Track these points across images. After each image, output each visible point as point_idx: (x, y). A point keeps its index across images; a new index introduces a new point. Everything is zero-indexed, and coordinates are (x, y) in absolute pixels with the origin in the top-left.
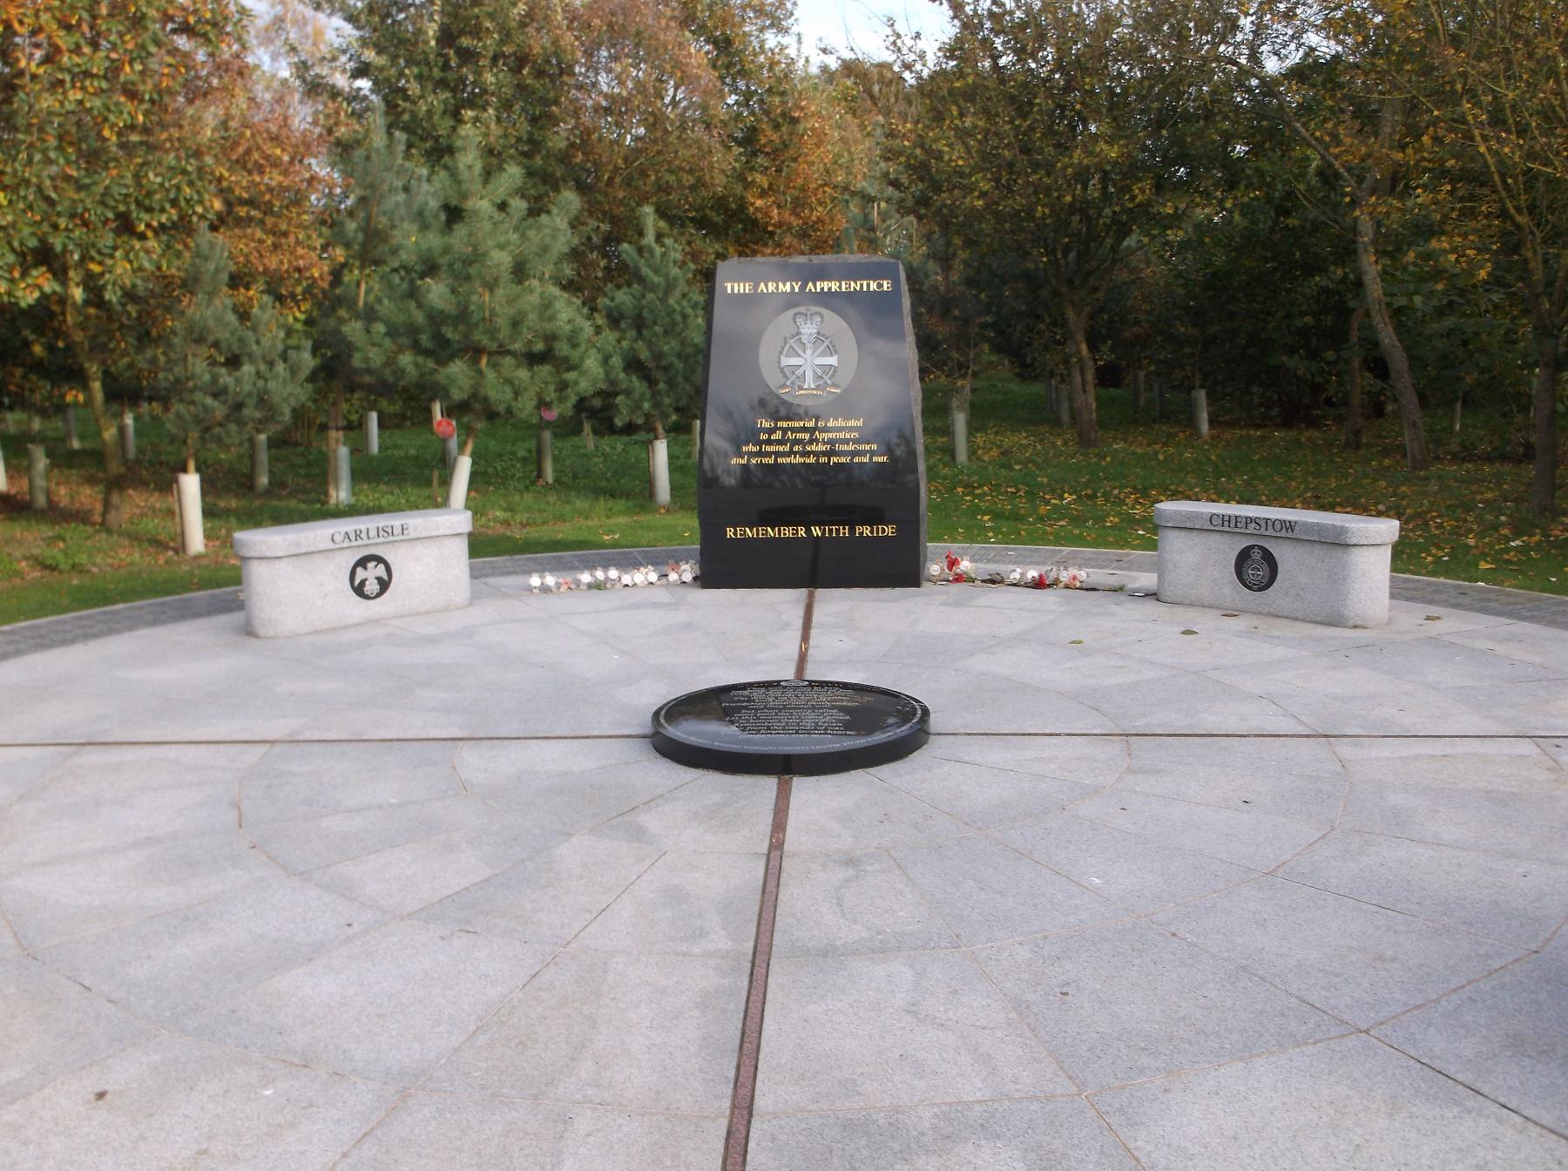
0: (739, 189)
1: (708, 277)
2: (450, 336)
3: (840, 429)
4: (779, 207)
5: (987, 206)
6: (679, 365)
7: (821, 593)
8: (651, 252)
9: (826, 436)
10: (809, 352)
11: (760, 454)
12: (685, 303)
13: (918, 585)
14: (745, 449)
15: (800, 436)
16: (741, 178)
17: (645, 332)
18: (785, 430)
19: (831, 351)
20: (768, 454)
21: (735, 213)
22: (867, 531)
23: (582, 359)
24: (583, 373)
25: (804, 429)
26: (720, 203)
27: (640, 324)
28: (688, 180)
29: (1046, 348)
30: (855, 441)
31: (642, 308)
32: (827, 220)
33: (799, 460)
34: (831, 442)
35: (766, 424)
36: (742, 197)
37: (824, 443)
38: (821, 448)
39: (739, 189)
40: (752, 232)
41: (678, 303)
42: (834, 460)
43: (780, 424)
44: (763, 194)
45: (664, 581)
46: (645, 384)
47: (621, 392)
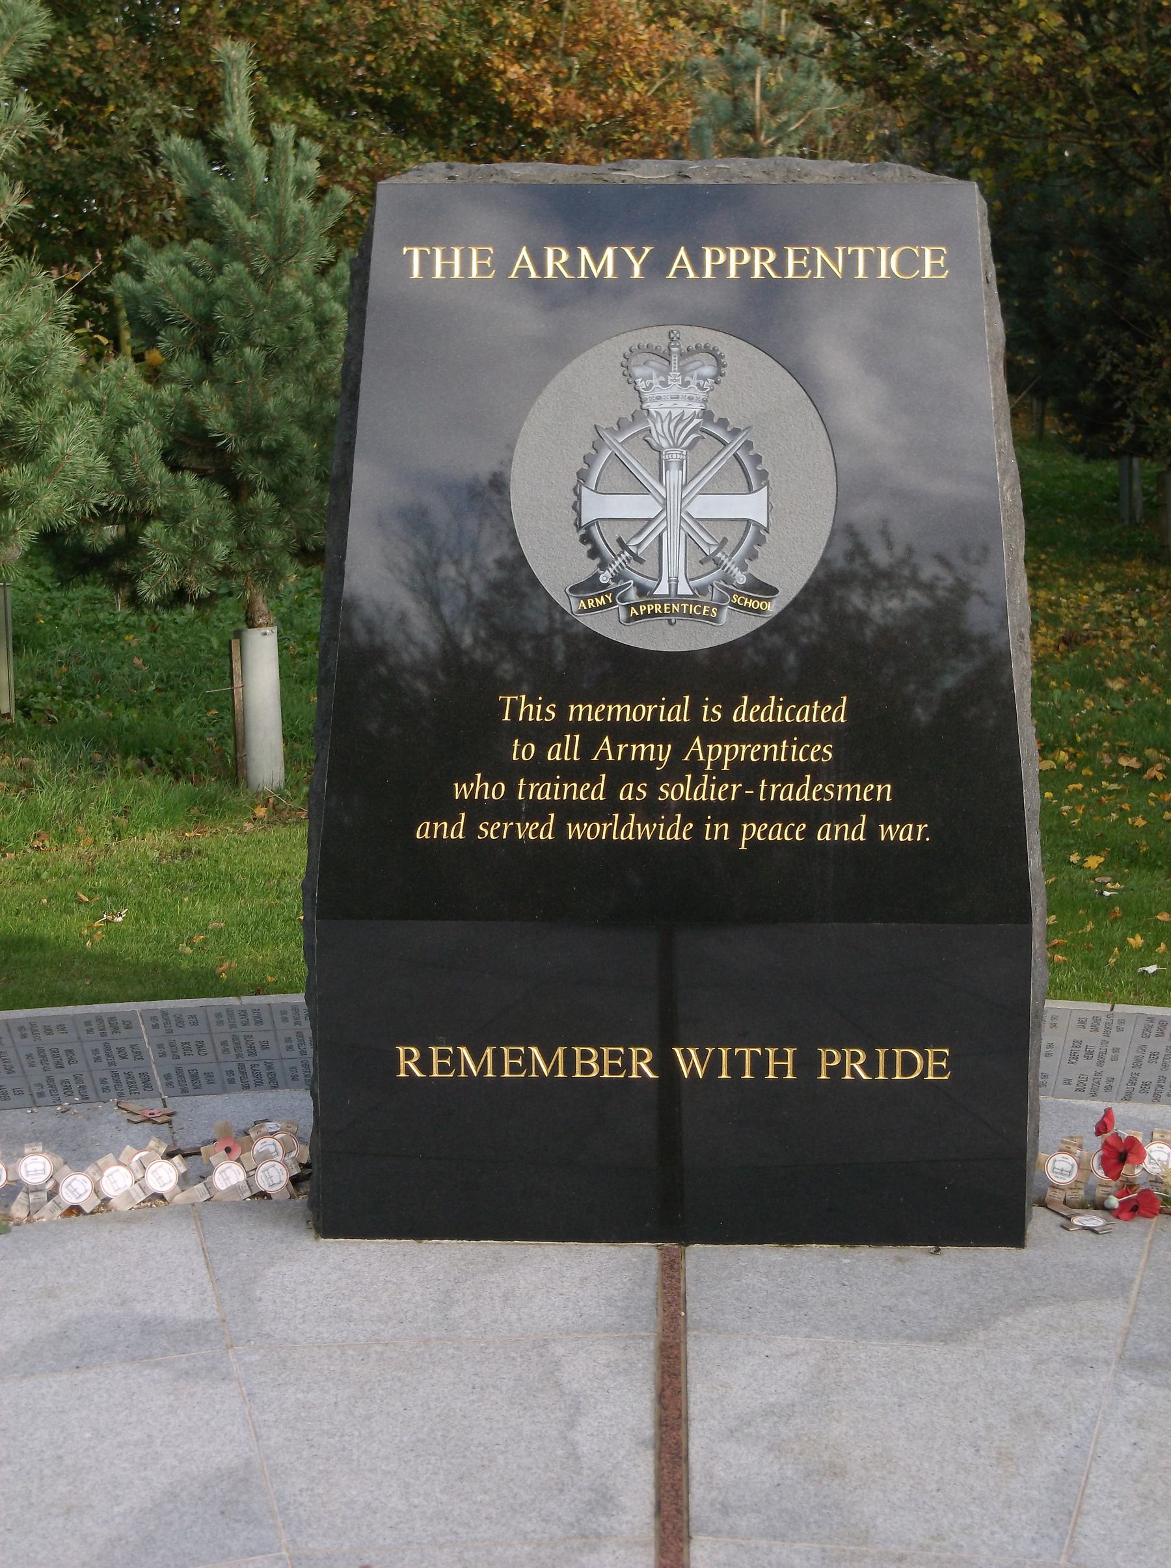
0: (473, 41)
1: (354, 234)
2: (235, 264)
4: (556, 82)
5: (1051, 69)
6: (305, 444)
7: (704, 1260)
8: (242, 157)
10: (674, 476)
11: (508, 809)
12: (324, 288)
14: (461, 790)
15: (640, 750)
17: (220, 360)
18: (591, 734)
19: (751, 473)
20: (538, 811)
21: (464, 91)
23: (48, 432)
24: (50, 472)
25: (651, 731)
27: (207, 341)
30: (819, 773)
31: (214, 299)
33: (636, 830)
34: (745, 772)
35: (532, 711)
36: (479, 59)
37: (720, 777)
38: (710, 792)
39: (473, 41)
40: (500, 132)
41: (309, 290)
42: (754, 831)
44: (523, 51)
45: (198, 1191)
46: (220, 493)
47: (158, 515)
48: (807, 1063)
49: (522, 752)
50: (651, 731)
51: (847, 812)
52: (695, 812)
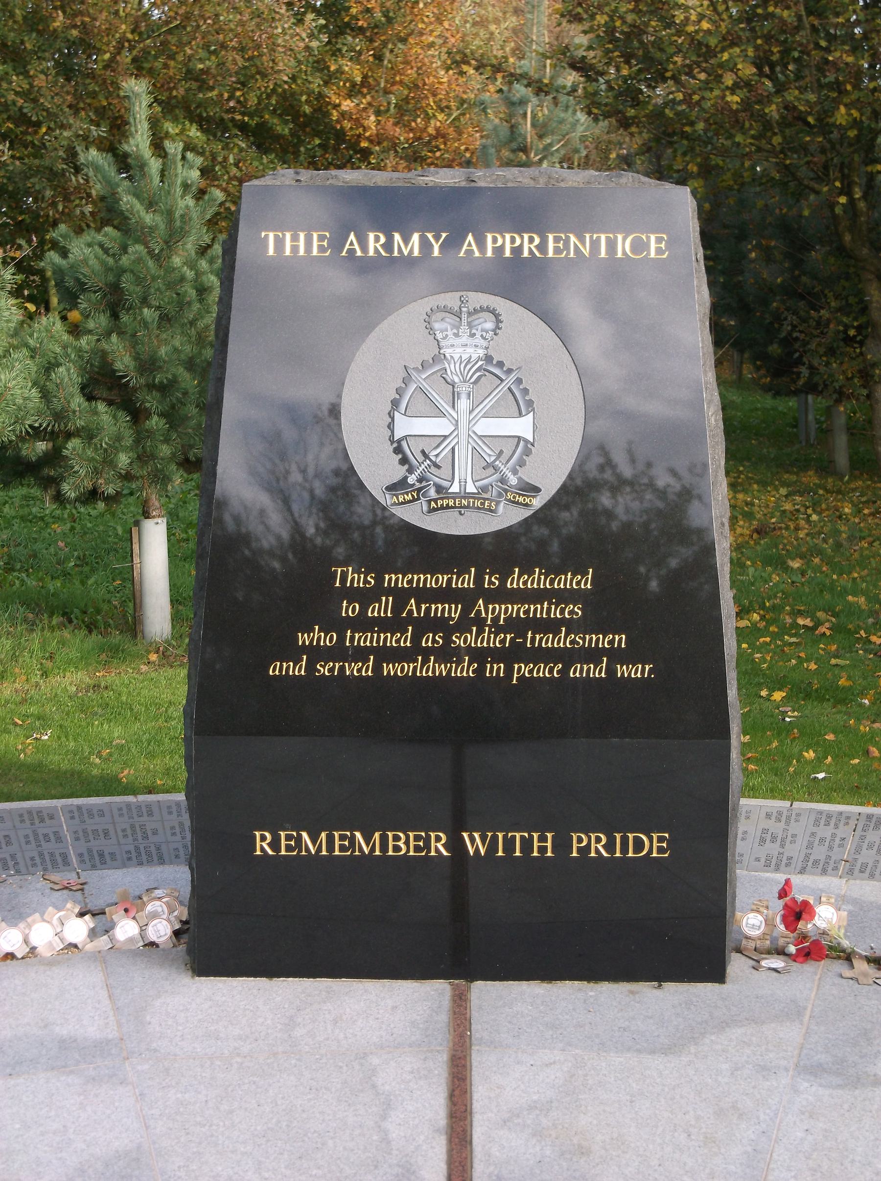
0: (316, 83)
3: (537, 596)
4: (378, 113)
5: (746, 105)
6: (188, 381)
8: (142, 166)
9: (504, 611)
10: (463, 404)
11: (339, 653)
12: (203, 264)
13: (718, 975)
14: (303, 639)
15: (438, 609)
16: (320, 66)
17: (125, 318)
18: (401, 596)
19: (521, 402)
20: (361, 654)
22: (598, 846)
25: (446, 595)
26: (288, 105)
27: (115, 302)
28: (235, 60)
29: (831, 351)
30: (571, 626)
32: (452, 134)
33: (435, 669)
34: (516, 626)
35: (356, 579)
36: (320, 96)
37: (497, 628)
39: (316, 83)
41: (192, 266)
43: (390, 579)
44: (353, 91)
45: (103, 942)
46: (124, 418)
48: (562, 845)
49: (349, 610)
50: (446, 595)
51: (592, 655)
52: (479, 656)
